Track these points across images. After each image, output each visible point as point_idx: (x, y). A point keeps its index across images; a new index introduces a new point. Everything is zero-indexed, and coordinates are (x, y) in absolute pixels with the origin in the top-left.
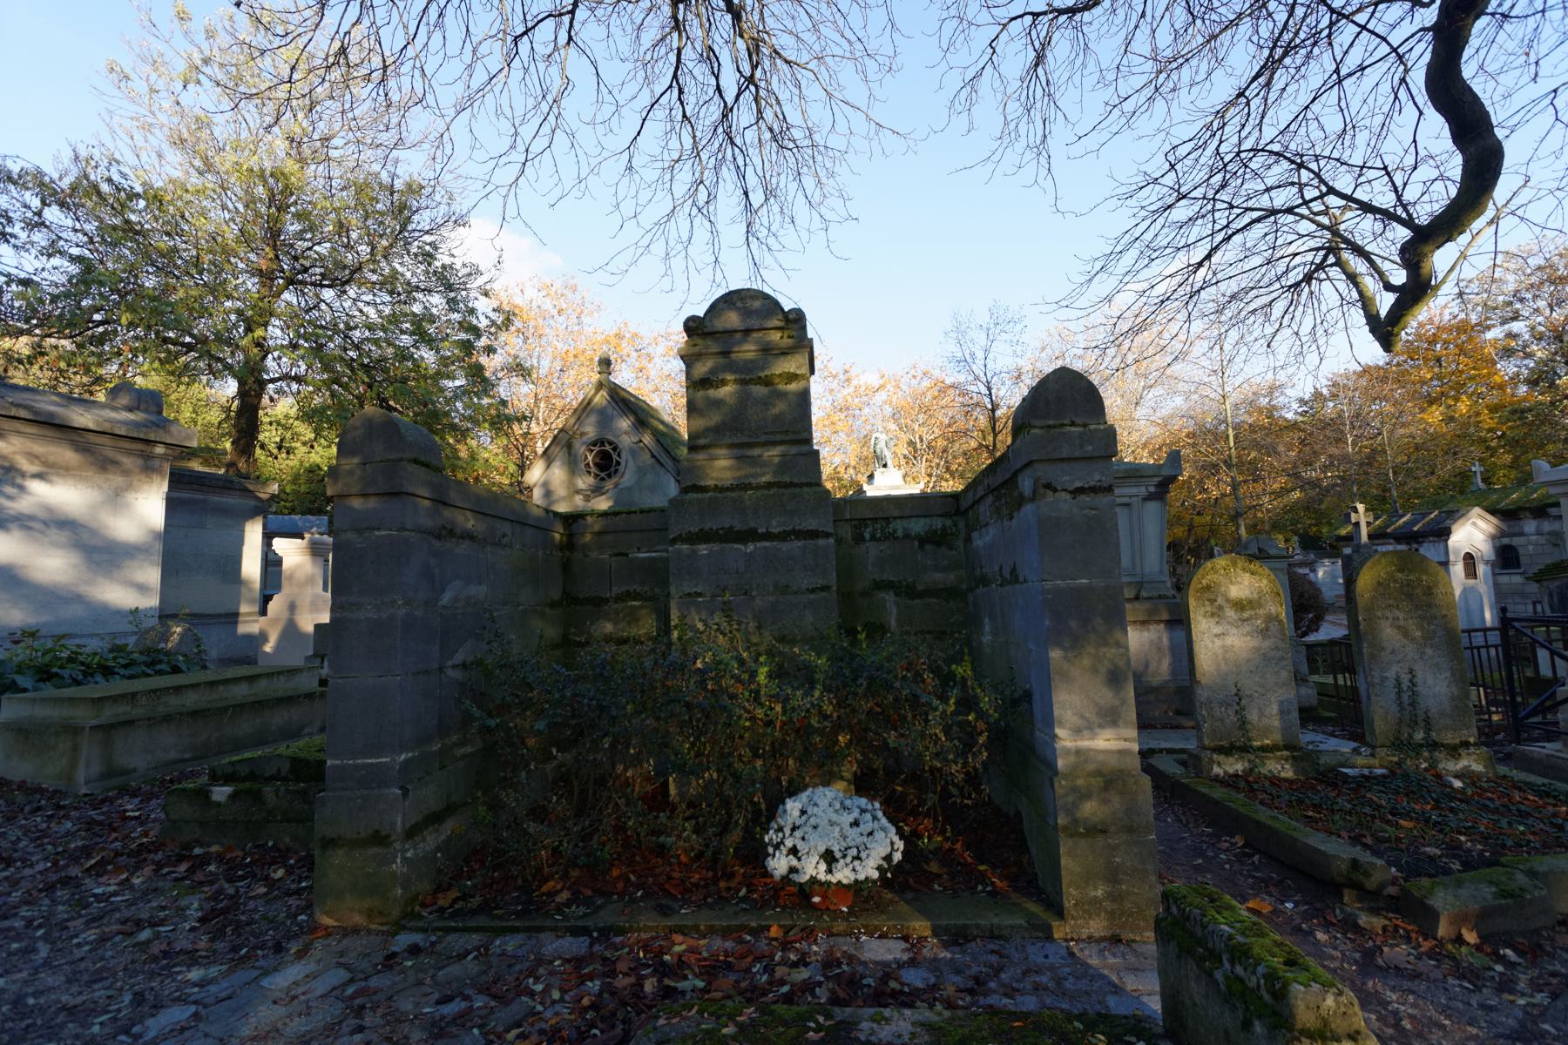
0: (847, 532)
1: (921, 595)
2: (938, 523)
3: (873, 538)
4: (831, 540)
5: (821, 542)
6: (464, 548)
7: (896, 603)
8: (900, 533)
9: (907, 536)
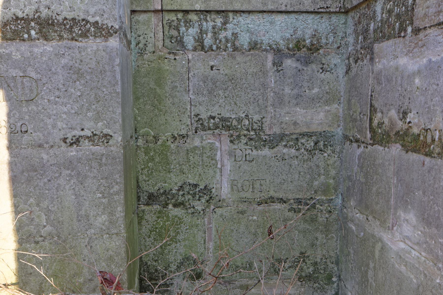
0: (152, 31)
1: (273, 142)
2: (308, 27)
3: (200, 45)
4: (114, 42)
5: (92, 45)
6: (198, 7)
7: (232, 154)
8: (244, 40)
9: (254, 46)
